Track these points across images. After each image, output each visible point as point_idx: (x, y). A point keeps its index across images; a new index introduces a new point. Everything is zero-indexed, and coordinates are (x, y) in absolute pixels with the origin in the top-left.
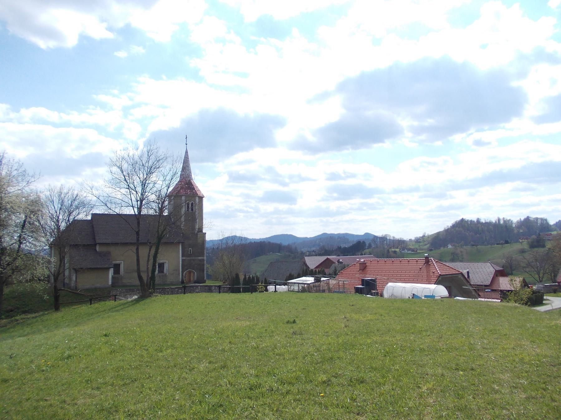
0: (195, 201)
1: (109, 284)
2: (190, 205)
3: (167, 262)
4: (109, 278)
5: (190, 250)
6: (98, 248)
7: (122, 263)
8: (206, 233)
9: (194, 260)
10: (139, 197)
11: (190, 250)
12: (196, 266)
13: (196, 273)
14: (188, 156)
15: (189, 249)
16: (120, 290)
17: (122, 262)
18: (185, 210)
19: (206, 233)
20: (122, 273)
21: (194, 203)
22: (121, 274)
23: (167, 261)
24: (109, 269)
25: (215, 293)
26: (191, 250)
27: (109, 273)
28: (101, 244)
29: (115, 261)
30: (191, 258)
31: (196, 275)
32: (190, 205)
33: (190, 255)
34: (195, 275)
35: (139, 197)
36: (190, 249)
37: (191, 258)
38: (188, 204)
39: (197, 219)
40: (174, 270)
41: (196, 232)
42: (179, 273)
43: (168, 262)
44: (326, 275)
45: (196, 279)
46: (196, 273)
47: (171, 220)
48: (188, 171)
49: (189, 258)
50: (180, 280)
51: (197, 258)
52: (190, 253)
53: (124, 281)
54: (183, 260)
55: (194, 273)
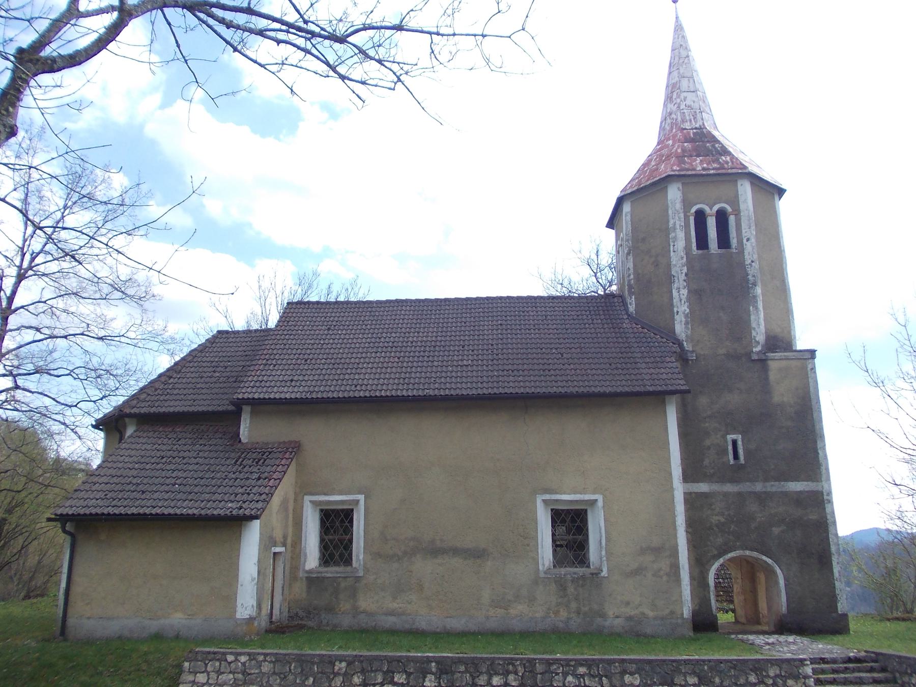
0: (735, 201)
1: (238, 616)
2: (711, 223)
3: (600, 503)
4: (236, 576)
5: (735, 443)
6: (246, 429)
7: (358, 502)
8: (812, 353)
9: (762, 498)
10: (281, 30)
11: (735, 443)
12: (776, 530)
13: (779, 571)
14: (686, 42)
15: (724, 437)
16: (243, 659)
17: (361, 497)
18: (687, 248)
19: (812, 353)
20: (358, 560)
21: (729, 209)
22: (354, 565)
23: (599, 498)
24: (240, 526)
25: (860, 547)
26: (740, 443)
27: (239, 550)
28: (261, 406)
29: (325, 494)
30: (745, 487)
31: (782, 582)
32: (711, 223)
33: (736, 473)
34: (777, 583)
35: (281, 30)
36: (734, 436)
37: (745, 487)
38: (700, 217)
39: (755, 284)
40: (643, 551)
41: (759, 348)
42: (675, 567)
43: (605, 497)
44: (759, 623)
45: (784, 609)
46: (779, 571)
47: (626, 310)
48: (690, 96)
49: (729, 488)
50: (687, 611)
51: (774, 487)
52: (732, 462)
53: (366, 603)
54: (691, 500)
55: (770, 572)
